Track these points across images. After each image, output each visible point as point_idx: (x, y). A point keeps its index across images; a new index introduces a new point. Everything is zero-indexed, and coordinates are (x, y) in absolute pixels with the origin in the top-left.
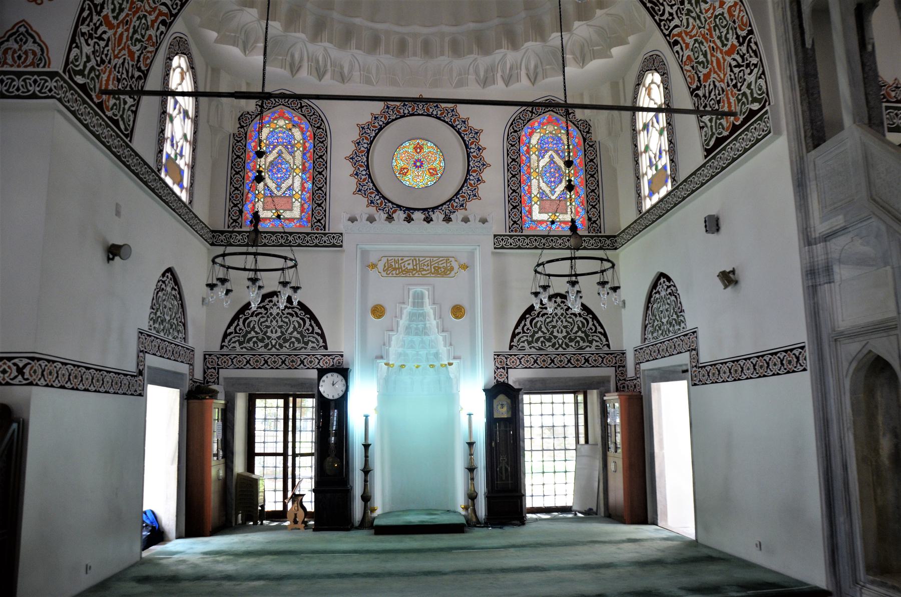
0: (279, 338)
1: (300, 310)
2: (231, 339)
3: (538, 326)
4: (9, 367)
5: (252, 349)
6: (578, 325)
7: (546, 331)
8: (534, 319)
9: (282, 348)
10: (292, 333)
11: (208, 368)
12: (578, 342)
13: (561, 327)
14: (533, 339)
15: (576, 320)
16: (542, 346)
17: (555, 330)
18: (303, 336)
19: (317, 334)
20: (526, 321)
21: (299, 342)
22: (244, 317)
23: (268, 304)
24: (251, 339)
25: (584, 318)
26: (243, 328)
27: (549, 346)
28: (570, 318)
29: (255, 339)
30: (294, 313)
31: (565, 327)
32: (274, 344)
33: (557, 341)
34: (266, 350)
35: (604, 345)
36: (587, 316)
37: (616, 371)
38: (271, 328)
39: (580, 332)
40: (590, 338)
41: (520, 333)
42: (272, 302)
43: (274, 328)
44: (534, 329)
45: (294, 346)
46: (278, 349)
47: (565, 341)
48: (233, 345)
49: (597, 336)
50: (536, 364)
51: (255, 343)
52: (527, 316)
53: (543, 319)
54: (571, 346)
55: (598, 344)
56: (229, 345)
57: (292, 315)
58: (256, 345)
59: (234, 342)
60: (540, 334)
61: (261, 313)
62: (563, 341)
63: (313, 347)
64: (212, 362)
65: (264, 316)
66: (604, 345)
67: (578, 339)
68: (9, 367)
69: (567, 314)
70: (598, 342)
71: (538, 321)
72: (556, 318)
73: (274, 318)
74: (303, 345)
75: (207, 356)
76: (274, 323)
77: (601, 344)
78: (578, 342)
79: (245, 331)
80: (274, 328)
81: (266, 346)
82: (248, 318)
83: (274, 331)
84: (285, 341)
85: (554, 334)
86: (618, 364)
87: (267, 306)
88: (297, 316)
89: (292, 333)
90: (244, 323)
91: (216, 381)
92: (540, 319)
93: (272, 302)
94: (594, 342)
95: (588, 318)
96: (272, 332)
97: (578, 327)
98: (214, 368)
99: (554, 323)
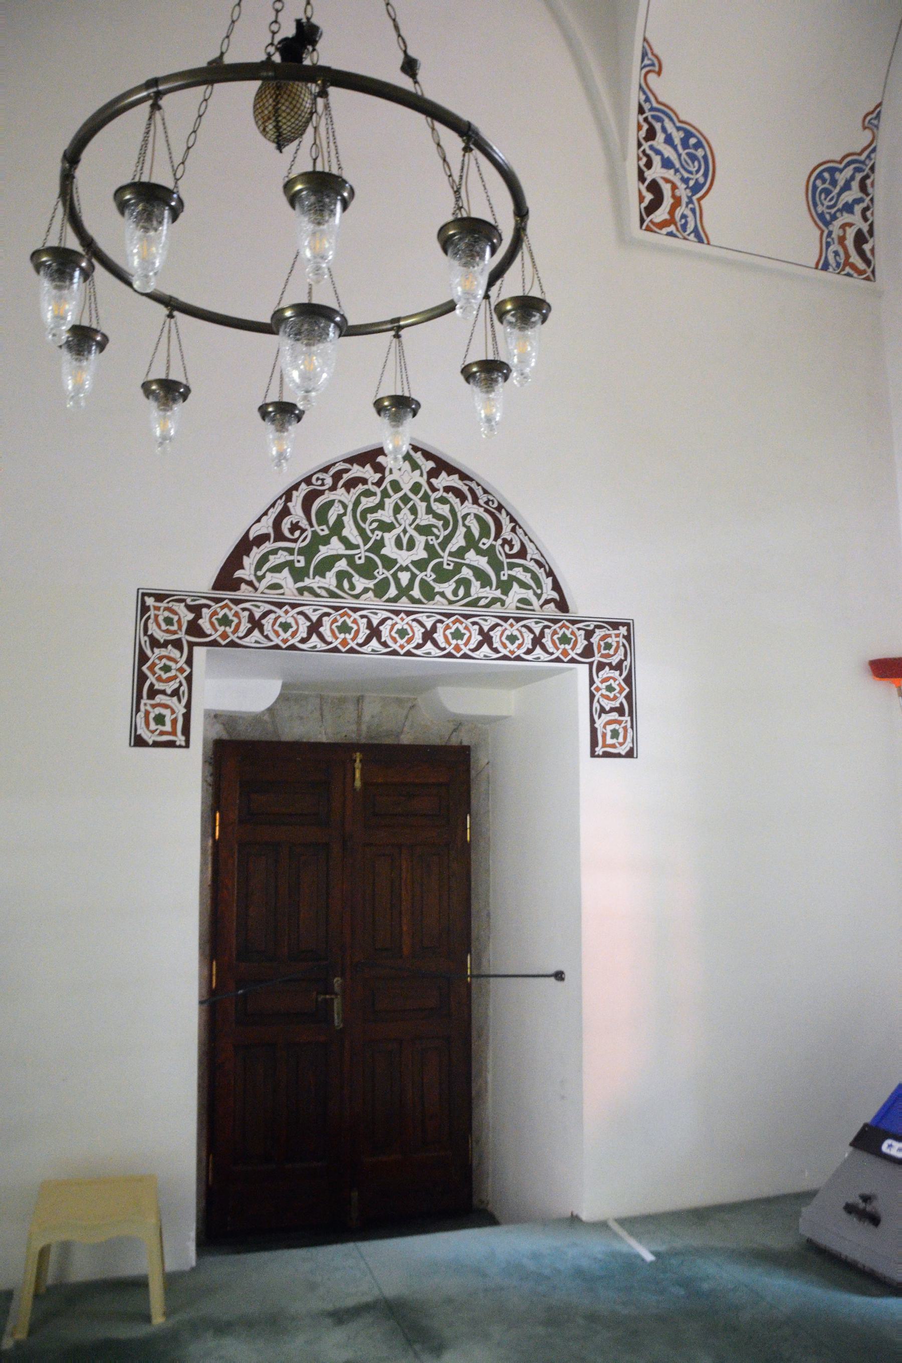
0: (421, 565)
2: (264, 559)
3: (332, 519)
4: (505, 647)
5: (333, 595)
6: (468, 528)
11: (155, 643)
12: (466, 583)
13: (411, 531)
14: (308, 562)
15: (461, 510)
16: (340, 586)
17: (389, 538)
18: (497, 566)
21: (485, 581)
24: (329, 562)
26: (304, 523)
27: (366, 590)
28: (443, 501)
29: (342, 565)
31: (424, 530)
33: (395, 575)
34: (379, 603)
35: (547, 602)
38: (395, 532)
39: (472, 552)
43: (405, 531)
44: (317, 528)
45: (467, 594)
47: (421, 575)
48: (271, 579)
49: (526, 569)
53: (349, 498)
54: (442, 594)
55: (529, 595)
56: (260, 579)
57: (463, 499)
58: (346, 585)
59: (277, 569)
60: (335, 547)
61: (364, 481)
62: (414, 576)
64: (608, 646)
65: (374, 489)
66: (547, 602)
67: (466, 573)
68: (505, 647)
69: (434, 490)
71: (331, 503)
72: (396, 497)
73: (405, 499)
74: (498, 593)
75: (150, 601)
76: (405, 515)
77: (539, 596)
78: (466, 583)
79: (309, 533)
80: (405, 531)
81: (381, 589)
82: (322, 493)
84: (443, 575)
89: (460, 553)
90: (306, 508)
91: (184, 688)
92: (340, 494)
94: (515, 586)
96: (398, 543)
97: (469, 535)
98: (177, 644)
99: (386, 515)
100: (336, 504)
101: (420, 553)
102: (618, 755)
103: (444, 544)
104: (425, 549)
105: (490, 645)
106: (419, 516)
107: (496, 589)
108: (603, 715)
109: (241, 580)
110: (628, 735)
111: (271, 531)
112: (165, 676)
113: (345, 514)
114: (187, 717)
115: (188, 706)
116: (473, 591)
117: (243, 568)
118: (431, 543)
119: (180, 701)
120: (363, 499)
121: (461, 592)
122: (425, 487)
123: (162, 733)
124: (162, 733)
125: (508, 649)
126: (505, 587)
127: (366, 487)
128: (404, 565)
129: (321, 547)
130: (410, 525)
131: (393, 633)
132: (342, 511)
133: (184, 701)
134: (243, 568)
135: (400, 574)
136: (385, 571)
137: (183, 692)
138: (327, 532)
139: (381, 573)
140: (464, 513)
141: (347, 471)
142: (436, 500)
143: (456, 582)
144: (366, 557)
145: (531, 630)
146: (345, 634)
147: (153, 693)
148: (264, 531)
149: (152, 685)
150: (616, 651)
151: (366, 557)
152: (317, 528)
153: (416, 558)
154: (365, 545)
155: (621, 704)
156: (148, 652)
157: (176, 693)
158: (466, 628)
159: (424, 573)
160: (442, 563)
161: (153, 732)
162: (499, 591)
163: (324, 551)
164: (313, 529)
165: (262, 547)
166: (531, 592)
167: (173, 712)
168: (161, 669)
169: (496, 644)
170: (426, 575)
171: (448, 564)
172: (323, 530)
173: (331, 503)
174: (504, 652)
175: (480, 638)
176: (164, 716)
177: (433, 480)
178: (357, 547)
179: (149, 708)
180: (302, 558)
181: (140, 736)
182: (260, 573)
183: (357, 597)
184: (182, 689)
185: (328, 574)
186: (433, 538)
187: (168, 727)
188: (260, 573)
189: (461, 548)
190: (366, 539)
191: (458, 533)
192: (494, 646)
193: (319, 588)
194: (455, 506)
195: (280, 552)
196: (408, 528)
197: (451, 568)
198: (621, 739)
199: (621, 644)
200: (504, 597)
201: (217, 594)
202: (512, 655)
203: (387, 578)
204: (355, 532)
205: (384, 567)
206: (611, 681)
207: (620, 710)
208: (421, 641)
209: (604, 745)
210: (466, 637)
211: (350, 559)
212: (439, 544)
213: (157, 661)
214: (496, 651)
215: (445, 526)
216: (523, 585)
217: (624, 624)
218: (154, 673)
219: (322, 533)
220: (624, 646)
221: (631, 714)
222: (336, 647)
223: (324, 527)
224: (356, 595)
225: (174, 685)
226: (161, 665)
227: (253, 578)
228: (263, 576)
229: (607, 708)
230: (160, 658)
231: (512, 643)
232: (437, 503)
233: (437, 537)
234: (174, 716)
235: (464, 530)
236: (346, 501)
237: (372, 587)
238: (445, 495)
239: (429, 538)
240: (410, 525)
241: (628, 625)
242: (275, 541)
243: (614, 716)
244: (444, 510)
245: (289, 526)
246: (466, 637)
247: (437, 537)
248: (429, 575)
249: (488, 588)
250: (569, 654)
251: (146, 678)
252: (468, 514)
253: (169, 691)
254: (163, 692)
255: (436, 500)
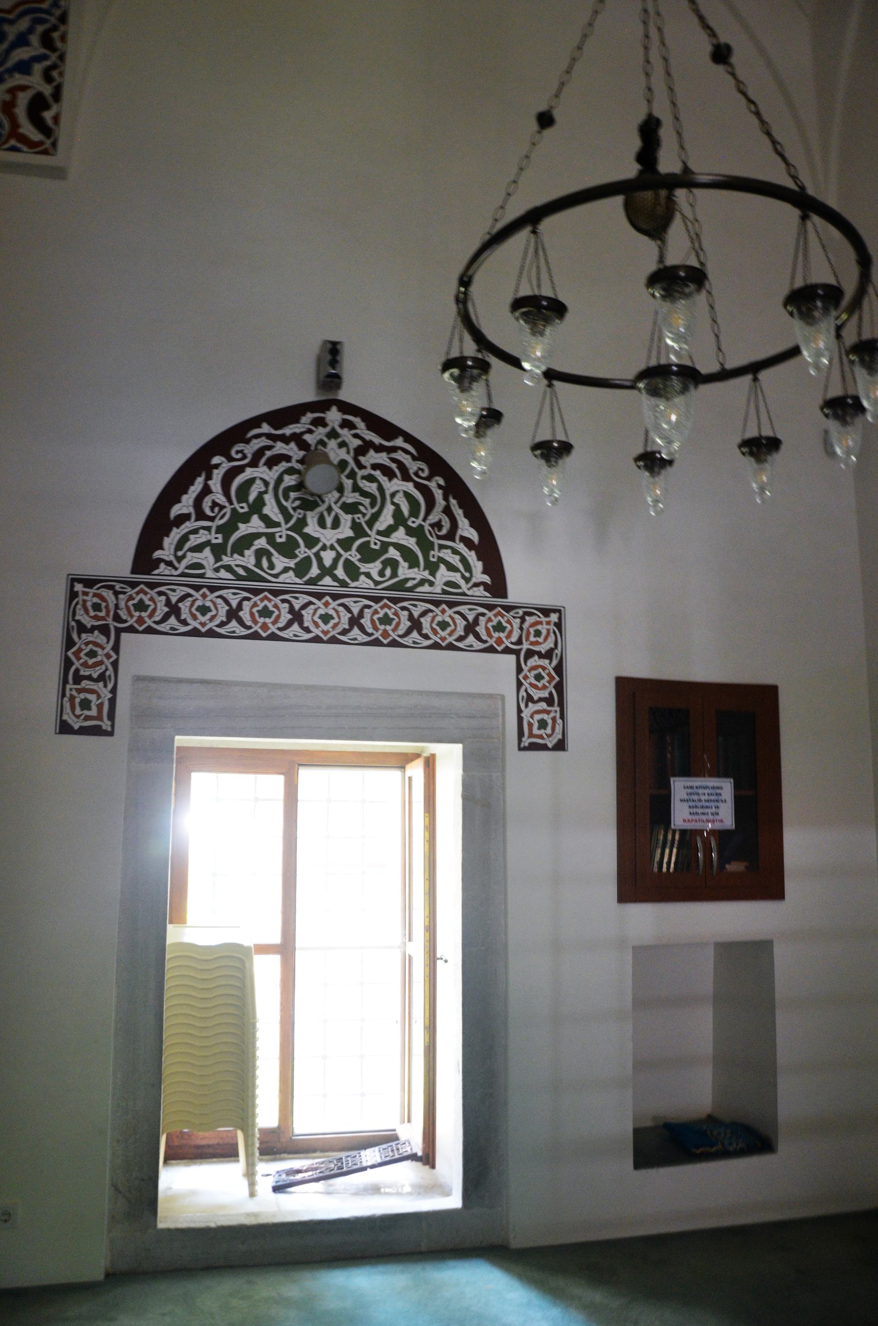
0: (346, 544)
1: (414, 458)
2: (184, 539)
3: (252, 497)
6: (397, 506)
7: (277, 517)
8: (240, 470)
9: (355, 578)
10: (389, 531)
11: (82, 628)
12: (393, 564)
13: (336, 509)
14: (226, 539)
16: (258, 565)
17: (312, 519)
18: (426, 546)
19: (467, 542)
20: (209, 477)
21: (413, 563)
22: (226, 465)
23: (310, 431)
24: (247, 541)
25: (418, 486)
26: (221, 499)
27: (286, 570)
28: (370, 478)
29: (261, 543)
30: (394, 466)
32: (328, 561)
35: (476, 585)
36: (428, 479)
37: (519, 670)
39: (402, 530)
40: (433, 558)
41: (185, 518)
42: (325, 425)
44: (236, 505)
45: (394, 574)
46: (343, 584)
47: (345, 555)
48: (192, 558)
50: (471, 639)
51: (260, 554)
52: (216, 460)
53: (271, 475)
54: (368, 575)
55: (456, 577)
56: (180, 559)
57: (389, 473)
58: (265, 563)
59: (199, 548)
60: (255, 524)
61: (288, 458)
62: (339, 556)
63: (449, 584)
66: (476, 585)
67: (393, 553)
69: (361, 466)
70: (456, 570)
71: (251, 481)
74: (426, 574)
75: (79, 587)
77: (467, 580)
78: (393, 564)
79: (228, 510)
80: (329, 509)
81: (302, 569)
83: (329, 521)
84: (368, 555)
85: (307, 530)
86: (525, 646)
87: (307, 437)
88: (406, 477)
89: (389, 531)
91: (110, 672)
92: (261, 472)
93: (325, 425)
94: (442, 567)
95: (432, 485)
96: (322, 523)
100: (258, 482)
101: (346, 531)
102: (544, 747)
103: (371, 523)
104: (352, 528)
105: (301, 625)
106: (346, 494)
107: (424, 570)
108: (530, 704)
109: (160, 560)
110: (557, 726)
111: (191, 510)
112: (91, 662)
113: (266, 492)
114: (113, 702)
115: (114, 691)
116: (400, 571)
117: (162, 549)
118: (358, 521)
119: (105, 686)
120: (286, 478)
121: (388, 572)
122: (352, 464)
123: (87, 718)
124: (87, 718)
125: (320, 629)
126: (432, 568)
127: (289, 465)
128: (328, 544)
129: (240, 525)
130: (336, 503)
131: (316, 618)
132: (263, 489)
133: (110, 686)
134: (162, 549)
135: (322, 554)
136: (307, 550)
137: (110, 676)
138: (246, 510)
139: (303, 552)
140: (393, 490)
141: (269, 448)
142: (363, 478)
143: (382, 562)
144: (288, 535)
145: (348, 609)
146: (385, 625)
147: (78, 679)
148: (185, 511)
149: (77, 670)
150: (546, 639)
151: (288, 535)
152: (236, 505)
153: (341, 536)
154: (287, 522)
155: (551, 694)
156: (75, 636)
157: (102, 678)
158: (276, 606)
159: (349, 553)
160: (369, 542)
161: (78, 717)
162: (247, 552)
163: (243, 529)
164: (232, 506)
165: (183, 526)
166: (458, 575)
167: (99, 697)
168: (86, 655)
169: (426, 630)
170: (350, 555)
171: (375, 544)
172: (242, 508)
173: (251, 481)
174: (316, 632)
175: (166, 609)
176: (90, 702)
177: (361, 459)
178: (278, 525)
179: (74, 693)
180: (220, 536)
181: (65, 721)
182: (180, 553)
183: (276, 576)
184: (108, 673)
185: (247, 552)
186: (360, 515)
187: (94, 712)
188: (180, 553)
189: (390, 526)
190: (287, 517)
191: (385, 511)
192: (183, 617)
193: (237, 566)
194: (383, 483)
195: (201, 531)
196: (333, 505)
197: (377, 547)
198: (549, 730)
199: (551, 631)
200: (431, 578)
201: (426, 597)
202: (203, 627)
203: (308, 558)
204: (276, 510)
205: (306, 547)
206: (540, 670)
207: (549, 701)
208: (462, 633)
209: (531, 735)
210: (394, 623)
211: (271, 538)
212: (366, 522)
213: (83, 647)
214: (307, 630)
215: (373, 505)
216: (451, 568)
217: (554, 611)
218: (79, 659)
219: (242, 511)
220: (554, 633)
221: (561, 704)
222: (131, 626)
223: (244, 505)
224: (274, 574)
225: (99, 670)
226: (88, 650)
227: (172, 558)
228: (184, 556)
229: (536, 698)
230: (87, 644)
231: (204, 614)
232: (364, 481)
233: (364, 515)
234: (100, 701)
235: (392, 508)
236: (267, 478)
237: (292, 566)
238: (373, 472)
239: (356, 516)
240: (336, 503)
241: (559, 611)
242: (196, 520)
243: (543, 705)
244: (372, 488)
245: (210, 504)
246: (317, 615)
247: (364, 515)
248: (353, 555)
249: (416, 570)
250: (146, 622)
251: (72, 664)
252: (398, 491)
253: (95, 676)
254: (89, 678)
255: (363, 478)
